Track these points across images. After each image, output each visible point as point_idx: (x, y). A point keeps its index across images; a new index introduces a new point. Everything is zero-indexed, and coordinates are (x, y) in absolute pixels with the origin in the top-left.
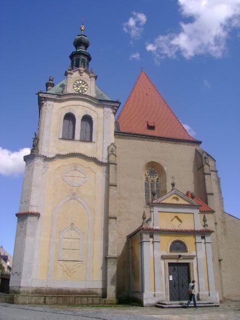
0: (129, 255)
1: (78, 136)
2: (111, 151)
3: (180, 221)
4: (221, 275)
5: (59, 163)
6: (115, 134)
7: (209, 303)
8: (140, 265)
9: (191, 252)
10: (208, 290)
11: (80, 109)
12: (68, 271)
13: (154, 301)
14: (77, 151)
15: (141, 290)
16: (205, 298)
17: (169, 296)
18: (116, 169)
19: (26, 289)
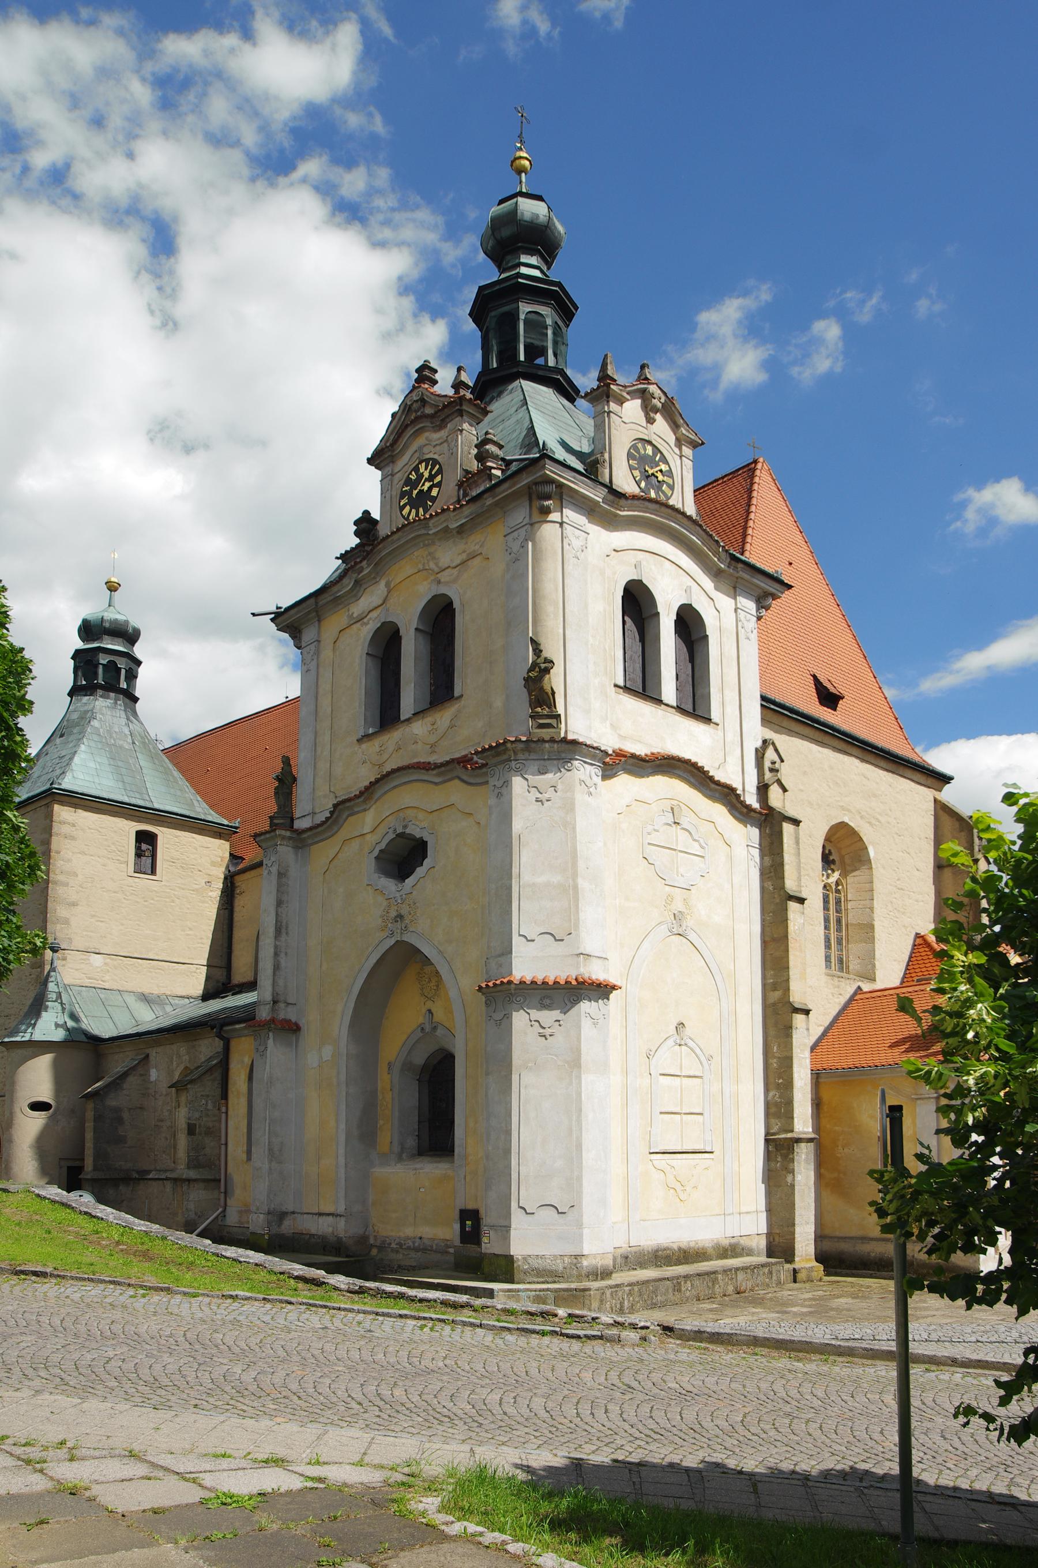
1: (669, 691)
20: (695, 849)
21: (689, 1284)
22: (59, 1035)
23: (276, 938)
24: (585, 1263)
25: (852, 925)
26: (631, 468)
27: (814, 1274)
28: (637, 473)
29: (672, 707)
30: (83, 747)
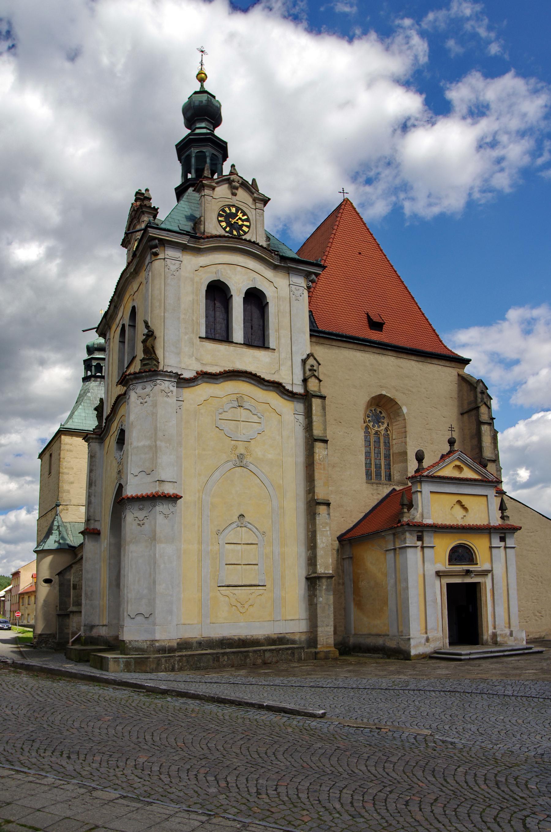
1: (238, 334)
2: (310, 371)
3: (465, 509)
5: (204, 390)
6: (311, 336)
9: (483, 564)
10: (507, 625)
11: (241, 274)
12: (239, 605)
20: (255, 419)
21: (226, 657)
22: (54, 546)
23: (89, 488)
24: (157, 644)
25: (395, 453)
26: (220, 222)
27: (331, 655)
28: (224, 224)
29: (240, 344)
30: (80, 407)
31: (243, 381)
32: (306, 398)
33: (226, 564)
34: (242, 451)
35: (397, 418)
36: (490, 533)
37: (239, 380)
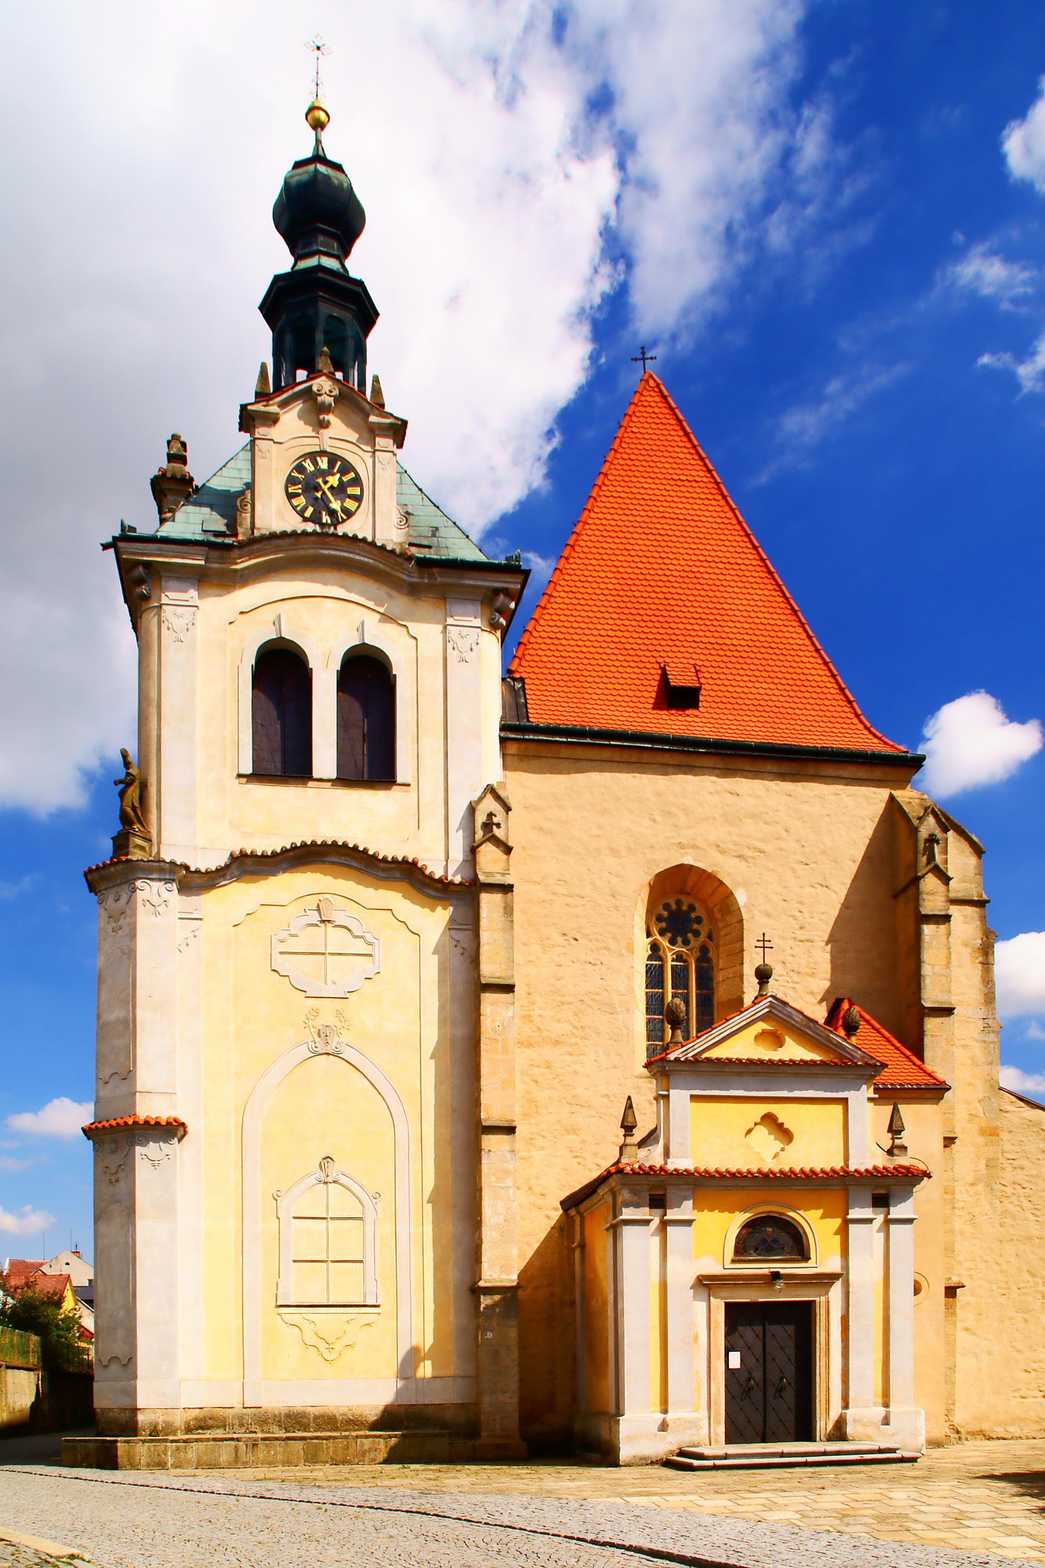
0: (572, 1276)
1: (325, 756)
2: (484, 831)
4: (950, 1343)
5: (239, 896)
6: (503, 741)
7: (880, 1451)
8: (611, 1313)
9: (824, 1257)
11: (327, 621)
12: (322, 1345)
13: (664, 1446)
14: (325, 832)
15: (612, 1409)
16: (870, 1431)
17: (721, 1429)
18: (508, 910)
19: (160, 1419)
26: (290, 496)
28: (301, 501)
31: (333, 863)
32: (463, 895)
33: (295, 1261)
34: (331, 1020)
35: (727, 918)
36: (846, 1190)
37: (324, 862)
